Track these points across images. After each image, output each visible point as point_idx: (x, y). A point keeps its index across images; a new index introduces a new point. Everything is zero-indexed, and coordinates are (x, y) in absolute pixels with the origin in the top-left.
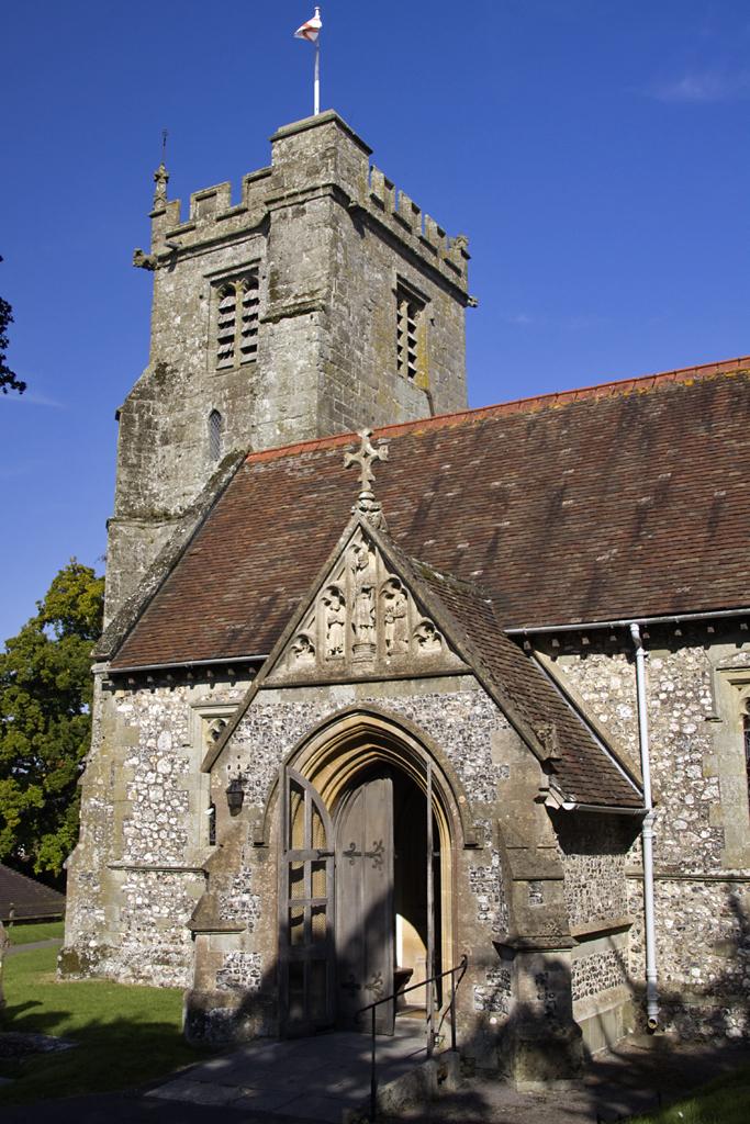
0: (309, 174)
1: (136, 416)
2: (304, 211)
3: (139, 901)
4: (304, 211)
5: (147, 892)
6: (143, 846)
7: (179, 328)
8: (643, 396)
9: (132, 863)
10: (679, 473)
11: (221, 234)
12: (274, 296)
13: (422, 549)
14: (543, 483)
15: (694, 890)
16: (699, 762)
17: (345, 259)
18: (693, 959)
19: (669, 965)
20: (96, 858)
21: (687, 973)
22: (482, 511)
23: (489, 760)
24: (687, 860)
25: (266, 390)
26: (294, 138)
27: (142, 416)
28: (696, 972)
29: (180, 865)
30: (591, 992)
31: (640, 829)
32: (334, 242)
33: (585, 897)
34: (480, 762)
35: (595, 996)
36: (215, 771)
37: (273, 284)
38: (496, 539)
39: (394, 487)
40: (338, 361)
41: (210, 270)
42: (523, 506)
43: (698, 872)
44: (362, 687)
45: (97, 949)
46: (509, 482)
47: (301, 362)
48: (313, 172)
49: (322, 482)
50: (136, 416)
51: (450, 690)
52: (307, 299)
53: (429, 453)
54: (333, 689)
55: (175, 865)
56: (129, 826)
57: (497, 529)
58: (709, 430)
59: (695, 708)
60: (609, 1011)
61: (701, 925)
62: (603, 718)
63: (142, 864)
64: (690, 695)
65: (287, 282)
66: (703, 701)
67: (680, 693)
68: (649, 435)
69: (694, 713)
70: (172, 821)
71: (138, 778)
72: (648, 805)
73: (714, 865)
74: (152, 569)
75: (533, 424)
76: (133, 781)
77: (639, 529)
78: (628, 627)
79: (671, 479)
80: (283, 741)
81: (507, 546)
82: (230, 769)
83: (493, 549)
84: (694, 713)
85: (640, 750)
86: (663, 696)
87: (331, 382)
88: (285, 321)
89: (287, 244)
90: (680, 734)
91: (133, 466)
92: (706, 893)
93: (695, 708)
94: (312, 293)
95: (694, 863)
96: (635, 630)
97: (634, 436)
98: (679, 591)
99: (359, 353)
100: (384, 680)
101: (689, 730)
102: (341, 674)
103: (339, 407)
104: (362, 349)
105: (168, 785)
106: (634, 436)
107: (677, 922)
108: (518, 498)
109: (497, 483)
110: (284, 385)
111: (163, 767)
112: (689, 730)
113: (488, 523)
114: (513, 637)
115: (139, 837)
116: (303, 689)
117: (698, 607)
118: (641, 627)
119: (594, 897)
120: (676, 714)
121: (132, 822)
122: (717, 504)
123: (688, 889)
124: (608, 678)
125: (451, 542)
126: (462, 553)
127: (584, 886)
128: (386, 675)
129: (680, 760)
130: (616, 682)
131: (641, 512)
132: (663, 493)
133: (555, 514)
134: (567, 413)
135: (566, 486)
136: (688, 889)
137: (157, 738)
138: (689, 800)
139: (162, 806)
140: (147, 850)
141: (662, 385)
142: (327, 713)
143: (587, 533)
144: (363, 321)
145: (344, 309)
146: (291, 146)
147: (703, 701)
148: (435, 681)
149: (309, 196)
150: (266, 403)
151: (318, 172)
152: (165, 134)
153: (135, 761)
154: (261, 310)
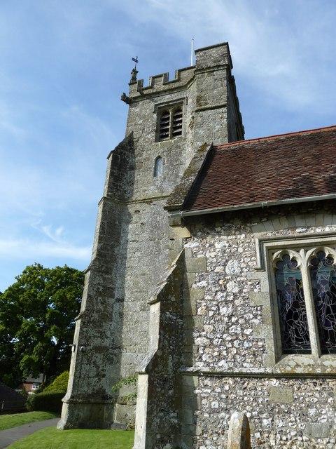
3: (215, 404)
5: (224, 396)
6: (216, 354)
9: (206, 369)
20: (170, 364)
29: (262, 370)
47: (218, 127)
55: (256, 370)
56: (200, 336)
63: (219, 370)
70: (248, 332)
71: (208, 297)
76: (203, 299)
105: (238, 302)
111: (232, 287)
121: (203, 333)
137: (225, 265)
139: (234, 319)
140: (220, 357)
153: (204, 283)
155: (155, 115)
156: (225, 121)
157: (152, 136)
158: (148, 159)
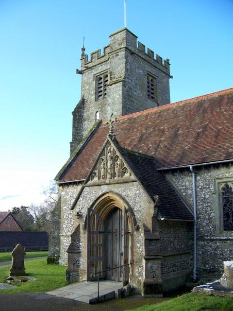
0: (119, 45)
1: (77, 114)
2: (118, 55)
4: (118, 55)
7: (88, 89)
8: (204, 100)
10: (211, 122)
11: (98, 63)
12: (111, 79)
13: (140, 147)
14: (174, 127)
15: (207, 243)
16: (210, 206)
17: (130, 67)
18: (207, 262)
19: (200, 264)
21: (205, 266)
22: (157, 135)
23: (140, 206)
24: (206, 234)
25: (109, 105)
26: (115, 36)
27: (78, 114)
28: (207, 266)
30: (174, 271)
31: (193, 226)
32: (126, 63)
33: (172, 245)
34: (138, 207)
35: (175, 272)
36: (74, 210)
37: (111, 75)
38: (159, 143)
39: (136, 130)
40: (129, 96)
41: (95, 73)
42: (168, 134)
43: (208, 238)
44: (109, 186)
45: (57, 257)
46: (166, 127)
48: (120, 44)
49: (118, 129)
50: (77, 114)
51: (131, 186)
52: (119, 79)
53: (146, 120)
54: (102, 186)
57: (160, 140)
58: (220, 109)
59: (209, 190)
60: (180, 277)
61: (209, 253)
62: (184, 194)
64: (207, 187)
65: (114, 75)
66: (211, 188)
67: (205, 186)
68: (204, 111)
69: (208, 192)
72: (195, 219)
73: (213, 236)
74: (177, 155)
75: (174, 110)
77: (197, 139)
78: (189, 167)
79: (208, 124)
80: (90, 201)
81: (162, 146)
82: (77, 209)
83: (158, 147)
84: (208, 192)
85: (196, 203)
86: (200, 187)
87: (126, 101)
88: (113, 85)
89: (114, 64)
90: (205, 198)
91: (76, 127)
92: (210, 244)
93: (209, 190)
94: (121, 77)
95: (208, 235)
96: (191, 168)
97: (200, 112)
98: (205, 156)
99: (135, 93)
100: (114, 184)
101: (207, 197)
102: (104, 182)
103: (129, 108)
104: (136, 92)
106: (200, 112)
107: (203, 252)
108: (167, 131)
109: (162, 127)
110: (113, 103)
112: (207, 197)
113: (157, 138)
114: (159, 171)
115: (67, 227)
116: (95, 187)
117: (209, 161)
118: (193, 167)
119: (176, 245)
120: (204, 192)
122: (219, 131)
123: (206, 243)
124: (185, 182)
125: (148, 145)
126: (150, 147)
127: (172, 242)
128: (115, 182)
129: (204, 206)
130: (187, 184)
131: (199, 134)
132: (205, 128)
133: (176, 135)
134: (184, 106)
135: (180, 127)
136: (206, 243)
138: (207, 217)
141: (209, 97)
142: (101, 193)
143: (183, 141)
144: (136, 84)
145: (130, 81)
146: (114, 38)
147: (211, 188)
148: (127, 183)
149: (119, 51)
150: (109, 108)
151: (121, 44)
152: (84, 38)
154: (108, 83)
155: (94, 82)
156: (121, 92)
157: (93, 98)
158: (92, 114)
